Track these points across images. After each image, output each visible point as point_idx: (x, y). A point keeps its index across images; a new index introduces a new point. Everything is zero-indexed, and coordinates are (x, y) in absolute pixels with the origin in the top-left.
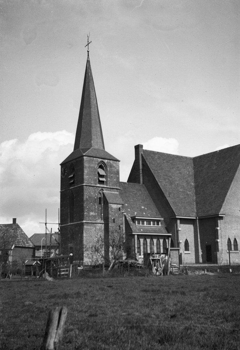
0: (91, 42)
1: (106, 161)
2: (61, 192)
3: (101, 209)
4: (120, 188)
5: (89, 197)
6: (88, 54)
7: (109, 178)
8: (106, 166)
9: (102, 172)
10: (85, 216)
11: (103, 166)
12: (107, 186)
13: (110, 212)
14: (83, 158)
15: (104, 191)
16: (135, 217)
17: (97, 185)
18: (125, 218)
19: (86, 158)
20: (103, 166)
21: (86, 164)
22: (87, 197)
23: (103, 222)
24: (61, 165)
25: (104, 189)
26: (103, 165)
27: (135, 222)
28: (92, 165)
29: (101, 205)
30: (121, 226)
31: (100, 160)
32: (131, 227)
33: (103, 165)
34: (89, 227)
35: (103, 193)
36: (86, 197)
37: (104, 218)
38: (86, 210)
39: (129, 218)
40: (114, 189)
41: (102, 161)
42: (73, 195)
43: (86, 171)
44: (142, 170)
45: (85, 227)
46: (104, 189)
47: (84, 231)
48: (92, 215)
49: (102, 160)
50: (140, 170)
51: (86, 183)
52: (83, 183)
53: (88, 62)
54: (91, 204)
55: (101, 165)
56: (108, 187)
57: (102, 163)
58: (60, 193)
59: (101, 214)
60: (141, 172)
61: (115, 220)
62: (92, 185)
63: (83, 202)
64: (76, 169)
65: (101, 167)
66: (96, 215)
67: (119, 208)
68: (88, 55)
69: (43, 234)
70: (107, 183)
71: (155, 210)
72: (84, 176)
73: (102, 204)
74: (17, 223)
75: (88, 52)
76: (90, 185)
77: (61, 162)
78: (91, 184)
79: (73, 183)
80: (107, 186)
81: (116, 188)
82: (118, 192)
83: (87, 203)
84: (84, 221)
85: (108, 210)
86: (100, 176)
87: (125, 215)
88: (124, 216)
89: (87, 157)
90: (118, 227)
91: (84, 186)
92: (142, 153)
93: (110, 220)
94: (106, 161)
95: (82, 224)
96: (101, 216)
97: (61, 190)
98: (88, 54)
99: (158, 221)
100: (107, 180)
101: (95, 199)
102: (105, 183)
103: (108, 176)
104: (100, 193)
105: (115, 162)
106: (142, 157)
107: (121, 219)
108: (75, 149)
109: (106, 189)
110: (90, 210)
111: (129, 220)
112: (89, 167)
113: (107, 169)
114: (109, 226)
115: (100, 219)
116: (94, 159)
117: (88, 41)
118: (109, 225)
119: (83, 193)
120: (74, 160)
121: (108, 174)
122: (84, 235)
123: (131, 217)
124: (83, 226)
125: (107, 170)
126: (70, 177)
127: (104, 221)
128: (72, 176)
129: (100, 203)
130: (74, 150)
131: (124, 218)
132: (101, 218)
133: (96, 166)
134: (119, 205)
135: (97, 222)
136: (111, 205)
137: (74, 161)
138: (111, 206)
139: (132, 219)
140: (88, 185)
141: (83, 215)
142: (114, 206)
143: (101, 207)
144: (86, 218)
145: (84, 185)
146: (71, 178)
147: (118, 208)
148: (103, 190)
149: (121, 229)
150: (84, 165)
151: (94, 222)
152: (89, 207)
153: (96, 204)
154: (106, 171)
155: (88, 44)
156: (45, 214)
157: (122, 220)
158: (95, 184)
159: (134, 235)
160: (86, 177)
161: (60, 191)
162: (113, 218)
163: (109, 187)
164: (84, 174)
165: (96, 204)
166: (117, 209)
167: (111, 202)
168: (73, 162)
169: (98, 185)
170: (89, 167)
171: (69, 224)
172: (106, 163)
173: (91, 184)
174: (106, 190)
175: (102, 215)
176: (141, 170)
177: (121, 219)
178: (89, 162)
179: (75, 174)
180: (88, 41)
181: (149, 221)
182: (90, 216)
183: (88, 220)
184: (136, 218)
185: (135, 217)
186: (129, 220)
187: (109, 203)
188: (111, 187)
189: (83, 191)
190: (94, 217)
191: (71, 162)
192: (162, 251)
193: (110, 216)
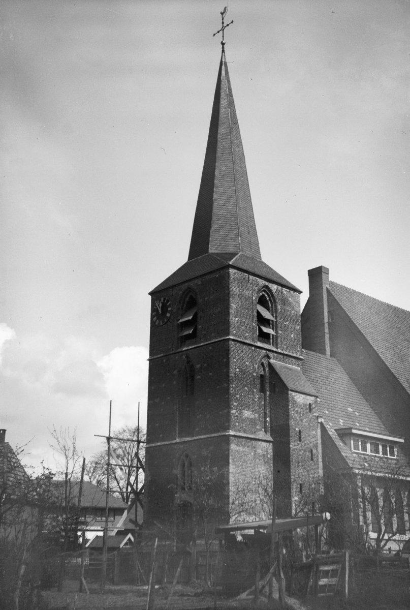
0: (232, 22)
1: (274, 287)
2: (150, 360)
3: (265, 406)
4: (302, 358)
5: (241, 371)
6: (223, 48)
7: (281, 330)
8: (275, 300)
9: (266, 314)
10: (233, 418)
11: (268, 298)
12: (277, 349)
13: (292, 413)
14: (229, 273)
15: (272, 361)
16: (351, 428)
17: (257, 343)
18: (322, 431)
19: (235, 273)
20: (268, 298)
21: (234, 289)
22: (238, 370)
23: (272, 440)
24: (150, 294)
25: (271, 355)
26: (266, 296)
27: (347, 442)
28: (246, 293)
29: (265, 394)
30: (314, 451)
31: (262, 282)
32: (344, 454)
33: (266, 296)
34: (241, 449)
35: (270, 365)
36: (234, 369)
37: (271, 427)
38: (235, 404)
39: (332, 433)
40: (291, 359)
41: (266, 287)
42: (192, 366)
43: (234, 306)
44: (329, 323)
45: (233, 447)
46: (271, 355)
47: (231, 457)
48: (248, 418)
49: (267, 283)
50: (323, 324)
51: (235, 335)
52: (228, 334)
53: (222, 64)
54: (246, 388)
55: (263, 295)
56: (279, 350)
57: (264, 291)
58: (148, 362)
59: (265, 418)
60: (327, 330)
61: (303, 434)
62: (247, 341)
63: (228, 382)
64: (200, 301)
65: (262, 301)
66: (255, 419)
67: (310, 404)
68: (223, 51)
69: (61, 482)
70: (277, 340)
71: (375, 420)
72: (231, 316)
73: (268, 393)
74: (6, 441)
75: (223, 44)
76: (243, 340)
77: (152, 288)
78: (246, 338)
79: (193, 336)
80: (277, 349)
81: (295, 355)
82: (298, 366)
83: (236, 387)
84: (232, 433)
85: (287, 406)
86: (262, 320)
87: (321, 423)
88: (319, 425)
89: (236, 271)
90: (308, 454)
91: (231, 342)
92: (328, 286)
93: (292, 434)
94: (274, 287)
95: (227, 440)
96: (266, 421)
97: (150, 355)
98: (223, 48)
99: (393, 444)
100: (277, 332)
101: (254, 378)
102: (271, 341)
103: (279, 325)
104: (262, 364)
105: (292, 292)
106: (328, 290)
107: (314, 432)
108: (192, 255)
109: (275, 354)
110: (243, 405)
111: (334, 436)
112: (241, 296)
113: (276, 306)
114: (289, 449)
115: (263, 430)
116: (251, 277)
117: (223, 23)
118: (291, 446)
119: (228, 359)
120: (197, 278)
121: (279, 320)
122: (232, 468)
123: (335, 430)
124: (228, 444)
125: (276, 309)
126: (181, 321)
127: (271, 436)
128: (190, 318)
129: (262, 390)
130: (190, 258)
131: (319, 431)
132: (265, 428)
133: (255, 298)
134: (308, 397)
135: (257, 438)
136: (294, 394)
137: (196, 281)
138: (293, 397)
139: (339, 435)
140: (239, 339)
141: (228, 416)
142: (300, 399)
143: (265, 400)
144: (235, 425)
145: (229, 339)
146: (187, 324)
147: (308, 403)
148: (269, 357)
149: (315, 459)
150: (231, 289)
151: (252, 436)
152: (241, 396)
153: (255, 391)
154: (274, 312)
155: (223, 29)
156: (112, 411)
157: (315, 436)
158: (253, 340)
159: (356, 475)
160: (234, 319)
161: (148, 357)
162: (297, 429)
163: (282, 352)
164: (231, 311)
165: (255, 391)
166: (305, 405)
167: (294, 387)
168: (191, 284)
169: (259, 344)
170: (241, 296)
171: (178, 440)
172: (274, 292)
173: (246, 338)
174: (276, 358)
175: (268, 419)
176: (326, 326)
177: (314, 432)
178: (242, 283)
179: (200, 314)
180: (223, 23)
181: (375, 442)
182: (242, 420)
183: (240, 431)
184: (354, 431)
185: (351, 428)
186: (334, 436)
187: (291, 390)
188: (285, 353)
189: (228, 354)
190: (253, 422)
191: (186, 284)
192: (395, 527)
193: (292, 423)
